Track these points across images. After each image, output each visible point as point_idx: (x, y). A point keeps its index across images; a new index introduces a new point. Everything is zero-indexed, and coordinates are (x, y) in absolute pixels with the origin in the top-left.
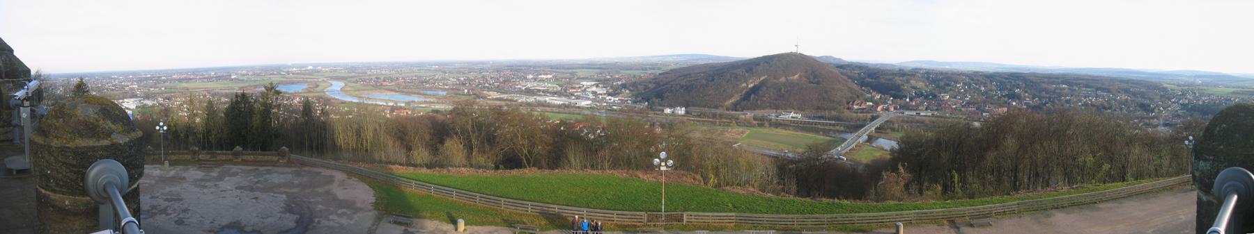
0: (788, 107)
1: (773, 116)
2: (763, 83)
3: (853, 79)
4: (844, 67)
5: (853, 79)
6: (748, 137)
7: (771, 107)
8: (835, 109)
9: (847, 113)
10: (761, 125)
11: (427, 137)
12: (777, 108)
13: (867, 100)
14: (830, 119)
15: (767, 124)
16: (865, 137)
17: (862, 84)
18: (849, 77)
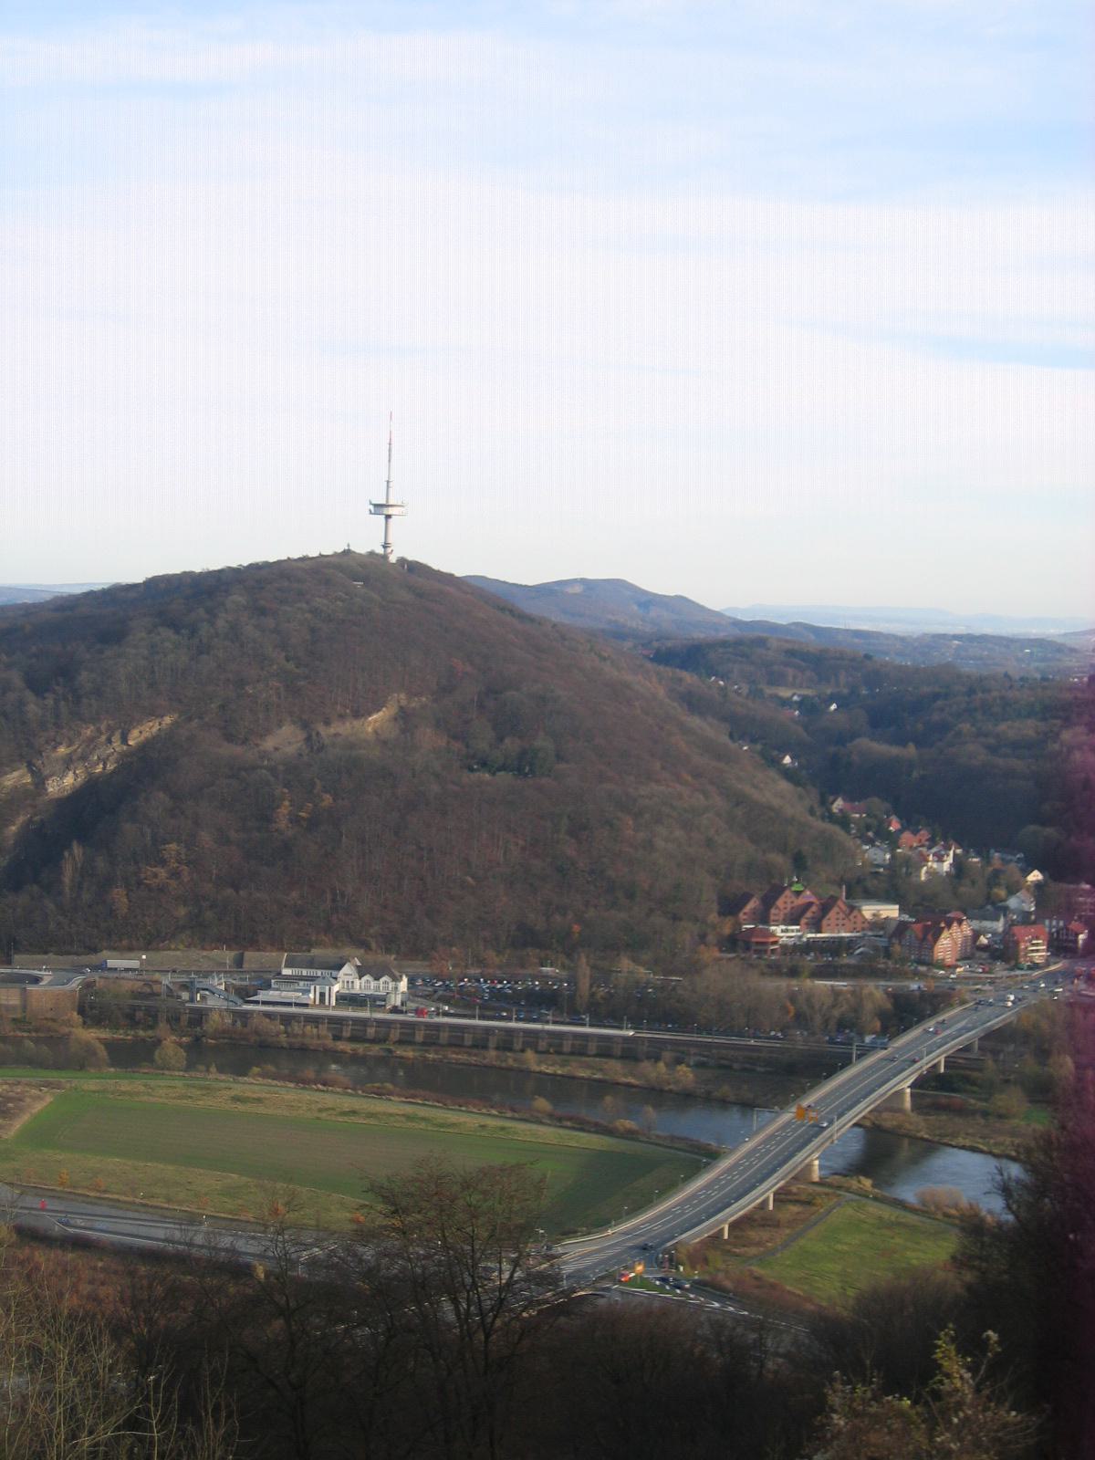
0: (323, 929)
1: (215, 995)
2: (144, 768)
3: (770, 744)
4: (708, 661)
5: (770, 744)
6: (40, 1135)
7: (201, 931)
8: (635, 944)
9: (719, 975)
10: (131, 1056)
11: (363, 719)
12: (242, 933)
13: (863, 887)
14: (605, 1012)
15: (171, 1046)
16: (843, 1134)
17: (831, 773)
18: (741, 727)
